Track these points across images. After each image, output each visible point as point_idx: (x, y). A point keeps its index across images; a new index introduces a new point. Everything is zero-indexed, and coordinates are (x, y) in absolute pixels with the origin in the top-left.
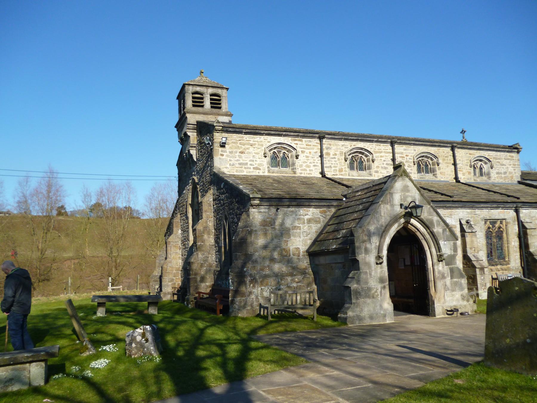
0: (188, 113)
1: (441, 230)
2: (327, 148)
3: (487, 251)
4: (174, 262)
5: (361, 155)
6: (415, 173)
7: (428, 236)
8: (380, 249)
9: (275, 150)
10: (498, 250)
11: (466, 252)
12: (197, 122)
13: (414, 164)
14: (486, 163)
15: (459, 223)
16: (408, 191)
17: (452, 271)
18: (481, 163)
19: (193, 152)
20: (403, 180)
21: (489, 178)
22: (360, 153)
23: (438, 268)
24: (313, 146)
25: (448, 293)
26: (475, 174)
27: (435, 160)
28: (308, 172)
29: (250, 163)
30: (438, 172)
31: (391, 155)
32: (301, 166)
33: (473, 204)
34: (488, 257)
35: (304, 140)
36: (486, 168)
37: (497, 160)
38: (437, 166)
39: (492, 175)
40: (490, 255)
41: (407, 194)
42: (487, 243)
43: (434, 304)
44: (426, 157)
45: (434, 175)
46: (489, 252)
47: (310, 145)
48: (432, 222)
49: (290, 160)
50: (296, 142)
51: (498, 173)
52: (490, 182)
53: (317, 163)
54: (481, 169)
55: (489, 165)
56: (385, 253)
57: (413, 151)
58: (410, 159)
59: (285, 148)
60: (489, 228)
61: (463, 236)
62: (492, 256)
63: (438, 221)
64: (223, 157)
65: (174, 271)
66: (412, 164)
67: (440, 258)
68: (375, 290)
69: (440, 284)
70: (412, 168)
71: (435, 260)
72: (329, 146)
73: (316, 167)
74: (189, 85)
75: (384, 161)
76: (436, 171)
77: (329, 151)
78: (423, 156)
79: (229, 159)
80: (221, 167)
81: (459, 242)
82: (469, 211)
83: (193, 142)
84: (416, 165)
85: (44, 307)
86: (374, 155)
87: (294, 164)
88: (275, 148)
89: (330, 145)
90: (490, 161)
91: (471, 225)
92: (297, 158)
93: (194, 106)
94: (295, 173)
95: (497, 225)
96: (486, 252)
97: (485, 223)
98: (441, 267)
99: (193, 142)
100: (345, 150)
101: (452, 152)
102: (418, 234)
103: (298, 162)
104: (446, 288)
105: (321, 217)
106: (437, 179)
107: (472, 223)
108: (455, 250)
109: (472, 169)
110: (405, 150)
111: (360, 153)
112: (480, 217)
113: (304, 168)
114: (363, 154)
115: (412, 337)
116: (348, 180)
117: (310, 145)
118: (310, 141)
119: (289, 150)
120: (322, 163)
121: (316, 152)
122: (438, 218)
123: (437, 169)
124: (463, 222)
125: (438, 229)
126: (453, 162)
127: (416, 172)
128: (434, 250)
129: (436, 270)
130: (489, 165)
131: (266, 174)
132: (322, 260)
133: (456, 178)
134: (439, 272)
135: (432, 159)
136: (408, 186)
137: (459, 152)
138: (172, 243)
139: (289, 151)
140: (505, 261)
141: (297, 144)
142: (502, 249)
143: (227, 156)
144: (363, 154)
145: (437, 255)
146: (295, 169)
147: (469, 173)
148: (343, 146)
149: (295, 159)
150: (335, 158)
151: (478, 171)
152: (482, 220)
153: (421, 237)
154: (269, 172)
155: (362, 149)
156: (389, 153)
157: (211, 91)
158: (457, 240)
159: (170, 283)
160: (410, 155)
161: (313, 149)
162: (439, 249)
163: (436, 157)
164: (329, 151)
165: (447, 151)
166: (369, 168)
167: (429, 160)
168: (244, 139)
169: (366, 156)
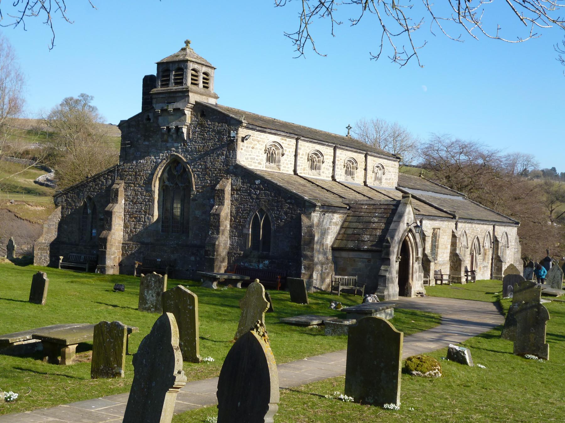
0: (192, 92)
4: (117, 234)
12: (196, 102)
14: (380, 169)
19: (185, 130)
21: (381, 182)
27: (355, 165)
28: (287, 169)
29: (256, 158)
31: (333, 158)
35: (288, 139)
43: (411, 288)
52: (381, 186)
59: (275, 146)
65: (117, 244)
71: (414, 261)
80: (240, 160)
85: (88, 275)
87: (279, 161)
90: (383, 168)
92: (243, 141)
93: (192, 83)
102: (409, 243)
103: (283, 159)
106: (354, 182)
115: (271, 322)
116: (312, 178)
118: (291, 141)
126: (364, 167)
128: (414, 254)
131: (264, 169)
132: (344, 254)
138: (117, 213)
139: (277, 149)
143: (245, 150)
157: (204, 69)
163: (356, 162)
166: (319, 169)
169: (318, 157)
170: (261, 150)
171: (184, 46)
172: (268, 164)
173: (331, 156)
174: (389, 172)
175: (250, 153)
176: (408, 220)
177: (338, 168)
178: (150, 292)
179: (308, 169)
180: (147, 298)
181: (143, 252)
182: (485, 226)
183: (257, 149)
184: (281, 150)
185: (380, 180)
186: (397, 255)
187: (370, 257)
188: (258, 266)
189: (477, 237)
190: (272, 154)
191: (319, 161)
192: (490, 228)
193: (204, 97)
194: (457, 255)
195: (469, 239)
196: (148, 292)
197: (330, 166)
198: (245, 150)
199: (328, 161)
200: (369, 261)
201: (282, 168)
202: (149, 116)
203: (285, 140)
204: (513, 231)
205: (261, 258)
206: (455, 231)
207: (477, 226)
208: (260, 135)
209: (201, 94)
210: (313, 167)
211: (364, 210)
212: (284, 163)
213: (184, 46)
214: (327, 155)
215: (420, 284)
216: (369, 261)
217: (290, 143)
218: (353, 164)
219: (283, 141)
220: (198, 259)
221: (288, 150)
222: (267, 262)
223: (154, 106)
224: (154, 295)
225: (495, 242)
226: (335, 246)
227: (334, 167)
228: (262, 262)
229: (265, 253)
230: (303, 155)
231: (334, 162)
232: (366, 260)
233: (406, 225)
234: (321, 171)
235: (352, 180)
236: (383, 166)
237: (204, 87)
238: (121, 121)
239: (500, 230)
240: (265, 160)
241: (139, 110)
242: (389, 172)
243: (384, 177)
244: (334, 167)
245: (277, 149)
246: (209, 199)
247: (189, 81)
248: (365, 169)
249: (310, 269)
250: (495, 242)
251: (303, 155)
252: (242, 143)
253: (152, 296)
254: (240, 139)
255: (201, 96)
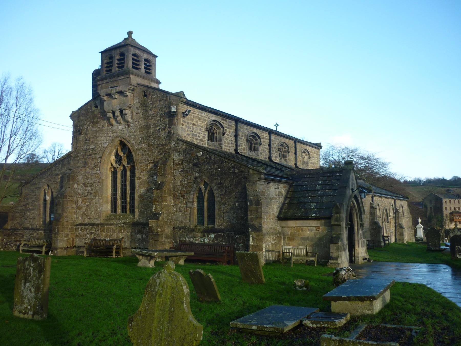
21: (308, 166)
27: (287, 149)
29: (198, 135)
31: (268, 141)
35: (228, 120)
45: (285, 160)
59: (217, 125)
64: (184, 127)
65: (70, 226)
66: (277, 150)
74: (132, 46)
75: (230, 141)
79: (186, 129)
82: (63, 155)
83: (131, 102)
86: (262, 140)
87: (221, 140)
90: (309, 154)
93: (133, 67)
94: (221, 147)
99: (131, 102)
101: (294, 144)
128: (359, 220)
131: (206, 146)
148: (246, 129)
154: (208, 145)
156: (267, 139)
157: (145, 56)
159: (66, 239)
163: (288, 147)
166: (257, 150)
168: (196, 112)
169: (256, 140)
170: (202, 127)
171: (127, 36)
172: (210, 142)
173: (267, 139)
174: (313, 157)
175: (191, 129)
176: (352, 186)
177: (273, 151)
178: (28, 284)
179: (248, 149)
180: (25, 294)
181: (94, 233)
182: (390, 200)
183: (198, 126)
184: (222, 130)
185: (307, 163)
186: (346, 221)
187: (319, 225)
188: (204, 241)
189: (386, 209)
190: (213, 133)
191: (257, 144)
192: (392, 201)
193: (146, 81)
194: (377, 223)
195: (381, 210)
196: (25, 284)
197: (266, 148)
198: (186, 126)
199: (264, 143)
200: (318, 228)
201: (224, 147)
202: (96, 103)
203: (226, 121)
204: (405, 204)
205: (207, 232)
206: (372, 203)
207: (385, 199)
208: (201, 113)
209: (143, 78)
210: (251, 148)
211: (307, 179)
212: (225, 142)
213: (127, 36)
214: (263, 138)
215: (364, 250)
216: (318, 228)
217: (230, 124)
218: (285, 148)
219: (223, 121)
220: (144, 237)
221: (228, 130)
222: (212, 236)
223: (99, 92)
224: (33, 290)
225: (396, 212)
226: (282, 216)
227: (270, 149)
228: (208, 236)
229: (210, 226)
230: (242, 136)
231: (270, 145)
232: (315, 229)
233: (351, 190)
234: (259, 152)
235: (285, 162)
236: (308, 152)
237: (146, 72)
238: (75, 116)
239: (399, 203)
240: (206, 139)
241: (89, 97)
242: (313, 157)
243: (310, 161)
244: (270, 149)
245: (218, 128)
246: (153, 177)
247: (130, 65)
248: (296, 154)
249: (260, 240)
250: (396, 212)
251: (242, 136)
252: (182, 119)
253: (30, 290)
254: (180, 115)
255: (143, 80)
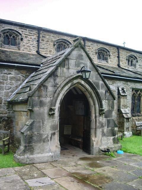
1: (104, 92)
2: (43, 37)
3: (132, 107)
5: (64, 44)
6: (96, 59)
7: (94, 95)
8: (53, 103)
9: (8, 34)
10: (137, 107)
11: (120, 108)
13: (96, 54)
15: (117, 89)
16: (82, 59)
17: (108, 121)
18: (132, 58)
20: (80, 50)
21: (135, 67)
22: (64, 42)
23: (99, 120)
24: (34, 34)
25: (105, 138)
26: (128, 64)
27: (108, 53)
30: (109, 60)
32: (24, 45)
33: (127, 80)
34: (132, 111)
35: (28, 29)
36: (134, 62)
37: (140, 58)
38: (109, 57)
39: (137, 66)
40: (133, 110)
41: (81, 61)
42: (132, 102)
44: (103, 51)
46: (133, 108)
47: (32, 33)
48: (98, 85)
49: (17, 41)
50: (22, 30)
51: (139, 65)
53: (35, 45)
54: (132, 62)
55: (136, 60)
56: (58, 105)
57: (96, 46)
58: (94, 50)
59: (14, 33)
60: (134, 94)
61: (119, 98)
62: (134, 110)
63: (102, 84)
67: (101, 112)
68: (46, 136)
69: (99, 131)
70: (95, 56)
71: (97, 114)
72: (44, 35)
73: (34, 48)
76: (108, 59)
77: (44, 39)
78: (101, 50)
81: (116, 102)
84: (97, 54)
87: (19, 44)
88: (8, 32)
89: (45, 35)
90: (136, 58)
91: (124, 91)
95: (138, 93)
96: (131, 108)
97: (133, 91)
98: (103, 119)
100: (54, 40)
104: (103, 134)
105: (21, 76)
107: (125, 90)
108: (113, 107)
109: (127, 61)
110: (92, 44)
111: (64, 42)
112: (130, 87)
113: (26, 47)
114: (66, 43)
117: (32, 33)
119: (17, 34)
120: (38, 46)
121: (35, 38)
122: (103, 83)
123: (109, 58)
124: (120, 89)
125: (102, 91)
126: (117, 56)
127: (97, 58)
129: (97, 121)
130: (136, 60)
133: (119, 65)
134: (100, 122)
135: (106, 53)
136: (82, 56)
137: (121, 51)
139: (17, 35)
140: (140, 114)
141: (22, 31)
142: (140, 107)
144: (66, 43)
145: (99, 110)
146: (20, 47)
147: (126, 63)
149: (20, 41)
150: (47, 43)
151: (130, 62)
152: (131, 89)
153: (88, 95)
155: (65, 40)
158: (115, 99)
160: (94, 48)
161: (33, 36)
162: (101, 105)
163: (109, 51)
164: (44, 39)
165: (115, 50)
167: (105, 53)
